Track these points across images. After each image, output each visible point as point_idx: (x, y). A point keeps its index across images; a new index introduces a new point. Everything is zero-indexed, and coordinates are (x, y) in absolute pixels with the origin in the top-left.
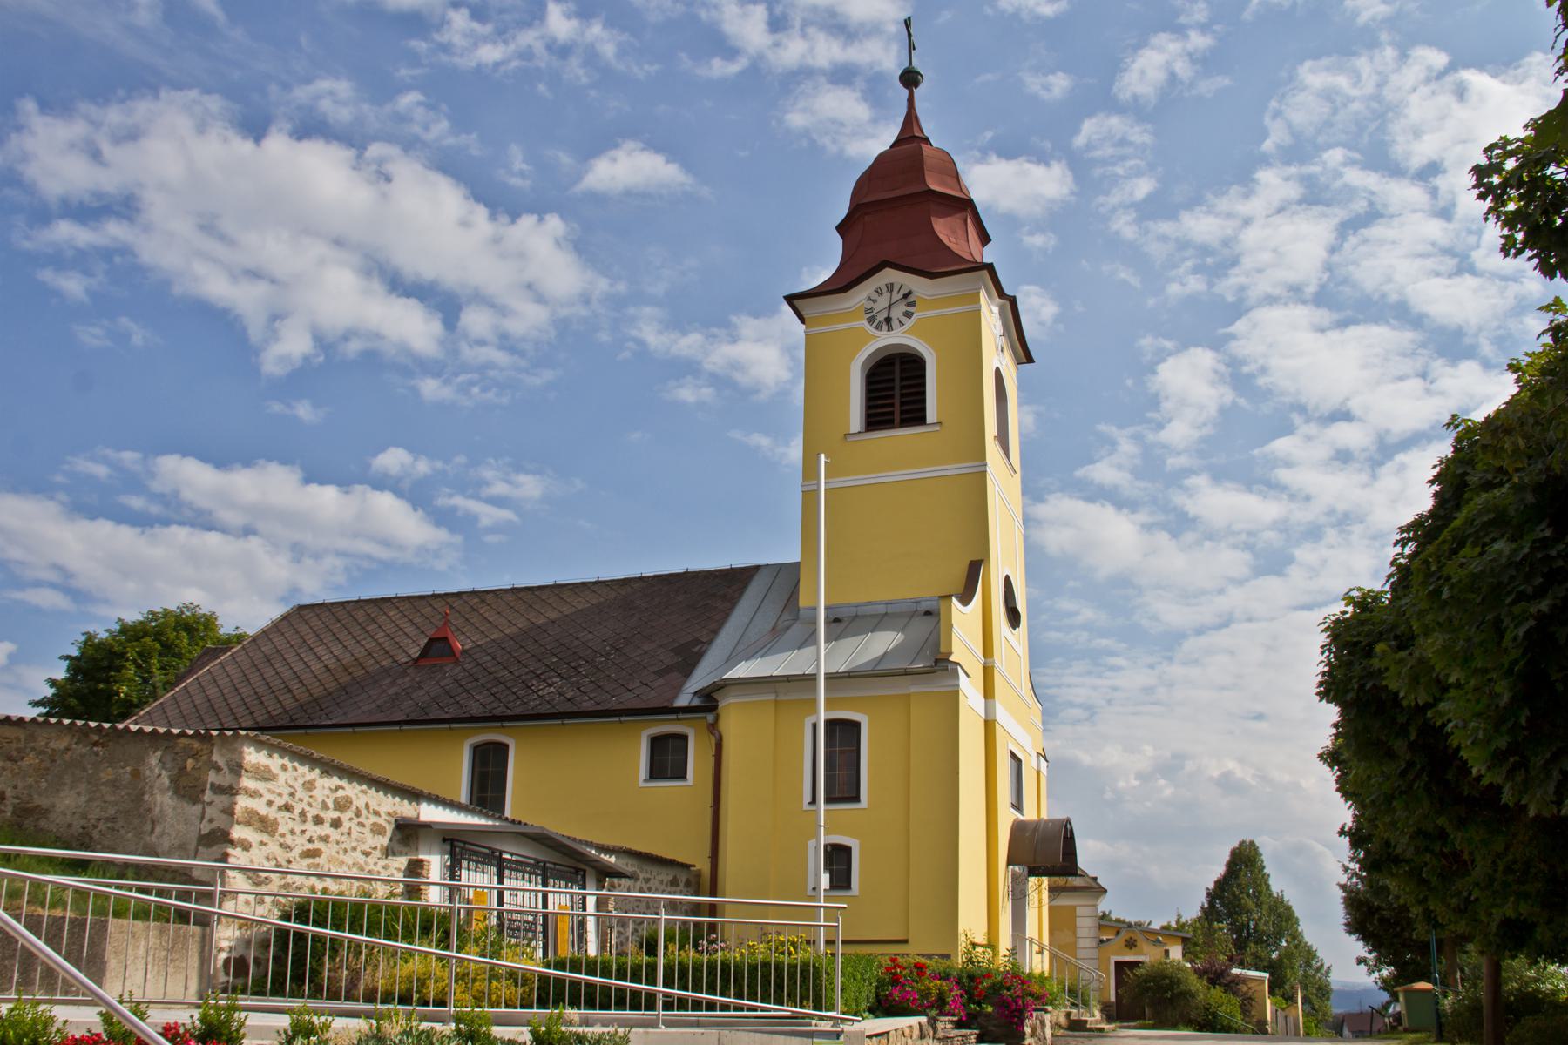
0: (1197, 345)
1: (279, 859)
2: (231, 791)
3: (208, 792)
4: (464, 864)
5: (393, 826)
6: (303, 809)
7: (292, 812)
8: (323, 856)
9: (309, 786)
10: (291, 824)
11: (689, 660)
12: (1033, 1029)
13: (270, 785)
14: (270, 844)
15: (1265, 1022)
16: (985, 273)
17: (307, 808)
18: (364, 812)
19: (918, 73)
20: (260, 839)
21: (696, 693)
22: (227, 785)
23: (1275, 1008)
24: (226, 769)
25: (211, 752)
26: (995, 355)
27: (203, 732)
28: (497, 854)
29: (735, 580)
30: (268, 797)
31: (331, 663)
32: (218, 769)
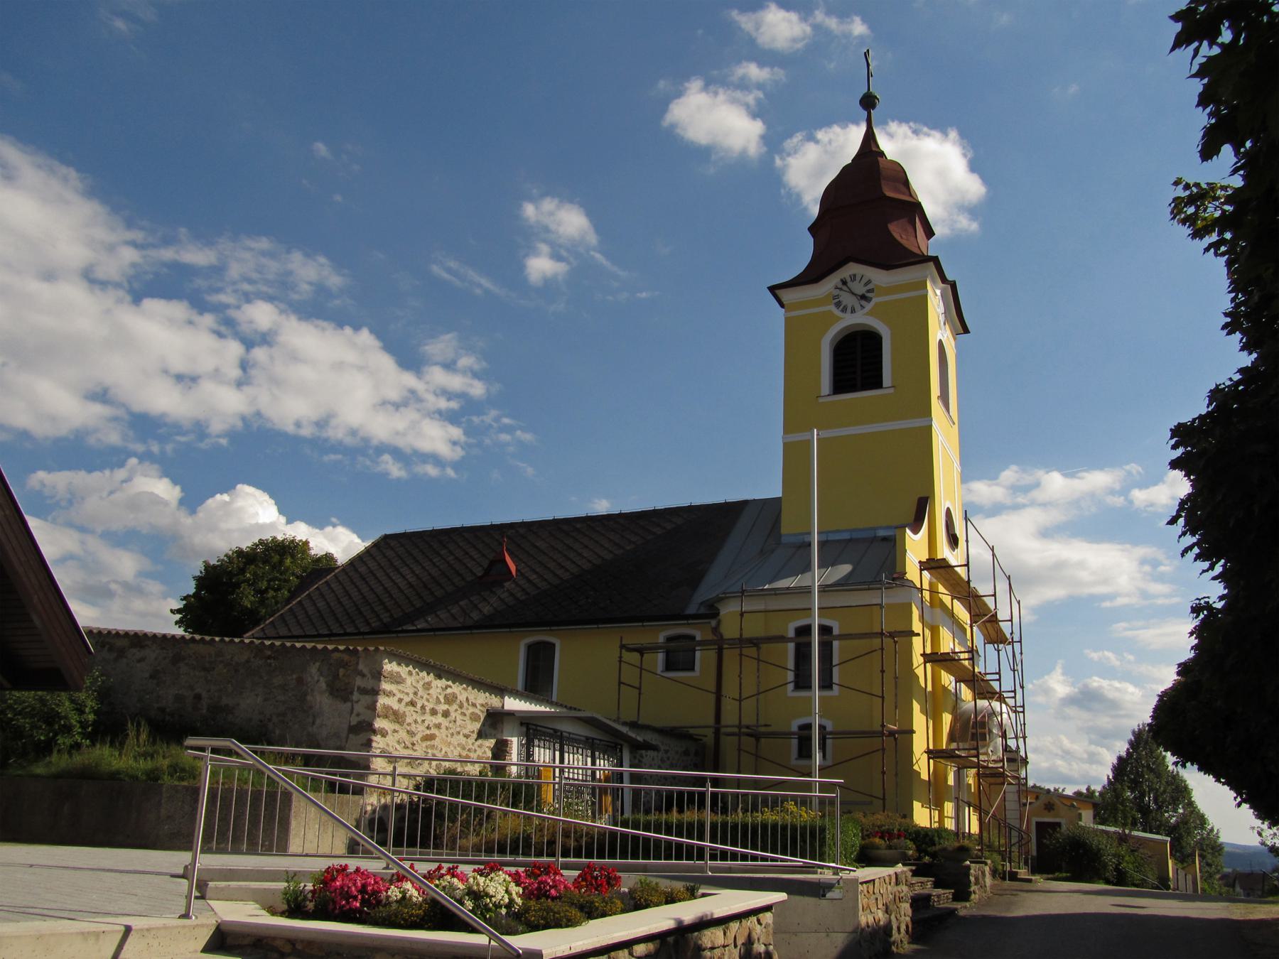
0: (296, 521)
1: (406, 743)
2: (375, 692)
3: (356, 693)
4: (536, 742)
5: (485, 714)
6: (423, 704)
7: (415, 707)
8: (437, 739)
9: (427, 686)
10: (415, 716)
11: (694, 582)
12: (977, 879)
13: (400, 687)
14: (401, 732)
15: (1168, 879)
16: (931, 264)
17: (426, 703)
18: (465, 704)
19: (876, 97)
20: (393, 728)
21: (701, 603)
22: (369, 688)
23: (1176, 867)
24: (369, 675)
25: (357, 663)
26: (939, 332)
27: (351, 648)
28: (559, 734)
29: (728, 513)
30: (399, 695)
31: (412, 579)
32: (363, 676)
